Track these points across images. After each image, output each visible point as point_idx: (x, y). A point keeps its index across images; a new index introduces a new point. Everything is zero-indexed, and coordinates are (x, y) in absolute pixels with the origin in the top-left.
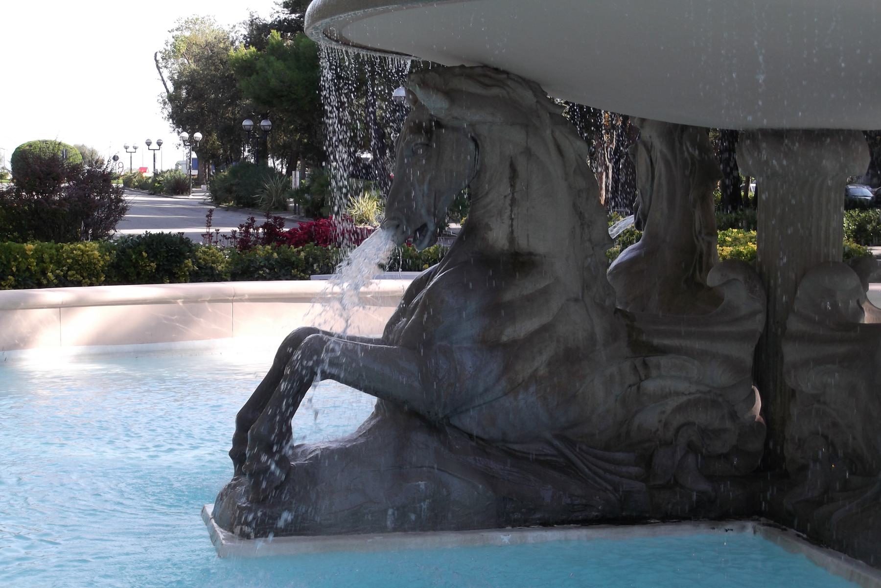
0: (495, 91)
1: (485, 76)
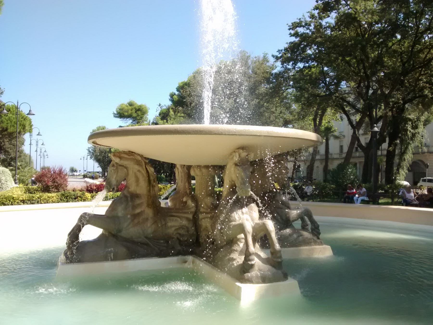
0: (131, 157)
1: (130, 153)
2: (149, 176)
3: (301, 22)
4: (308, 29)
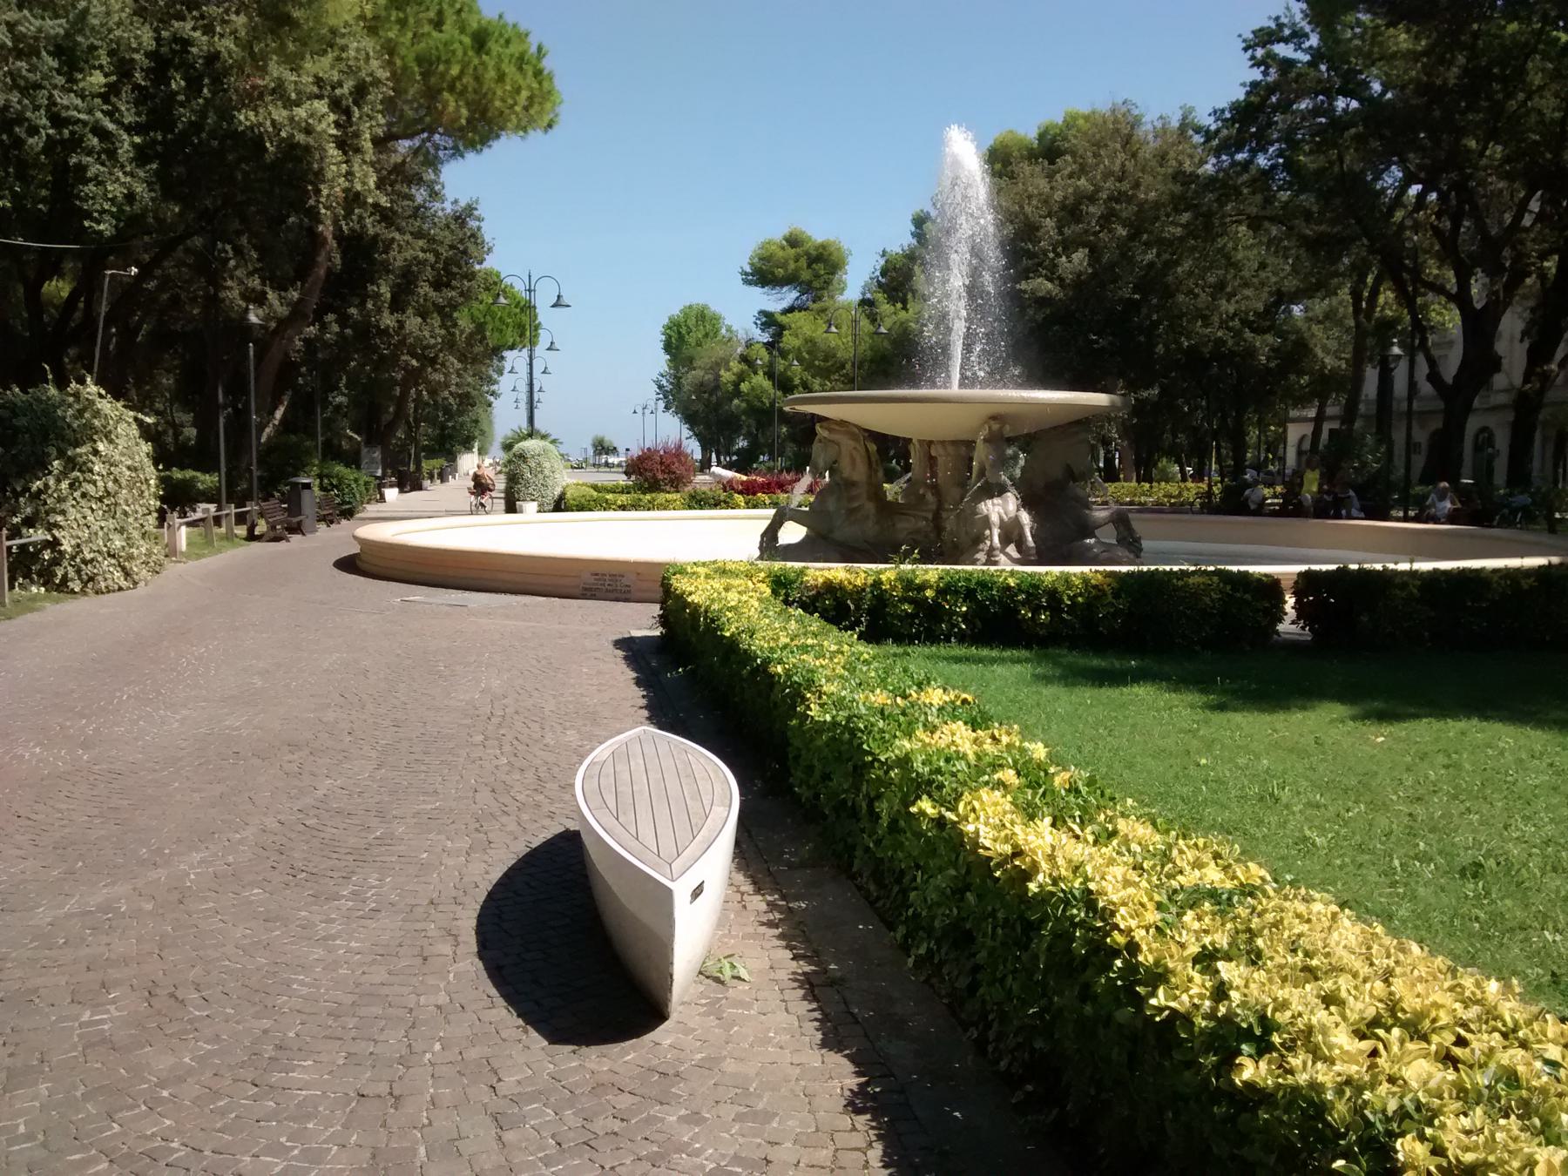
2: (869, 458)
3: (1281, 26)
4: (1298, 47)
